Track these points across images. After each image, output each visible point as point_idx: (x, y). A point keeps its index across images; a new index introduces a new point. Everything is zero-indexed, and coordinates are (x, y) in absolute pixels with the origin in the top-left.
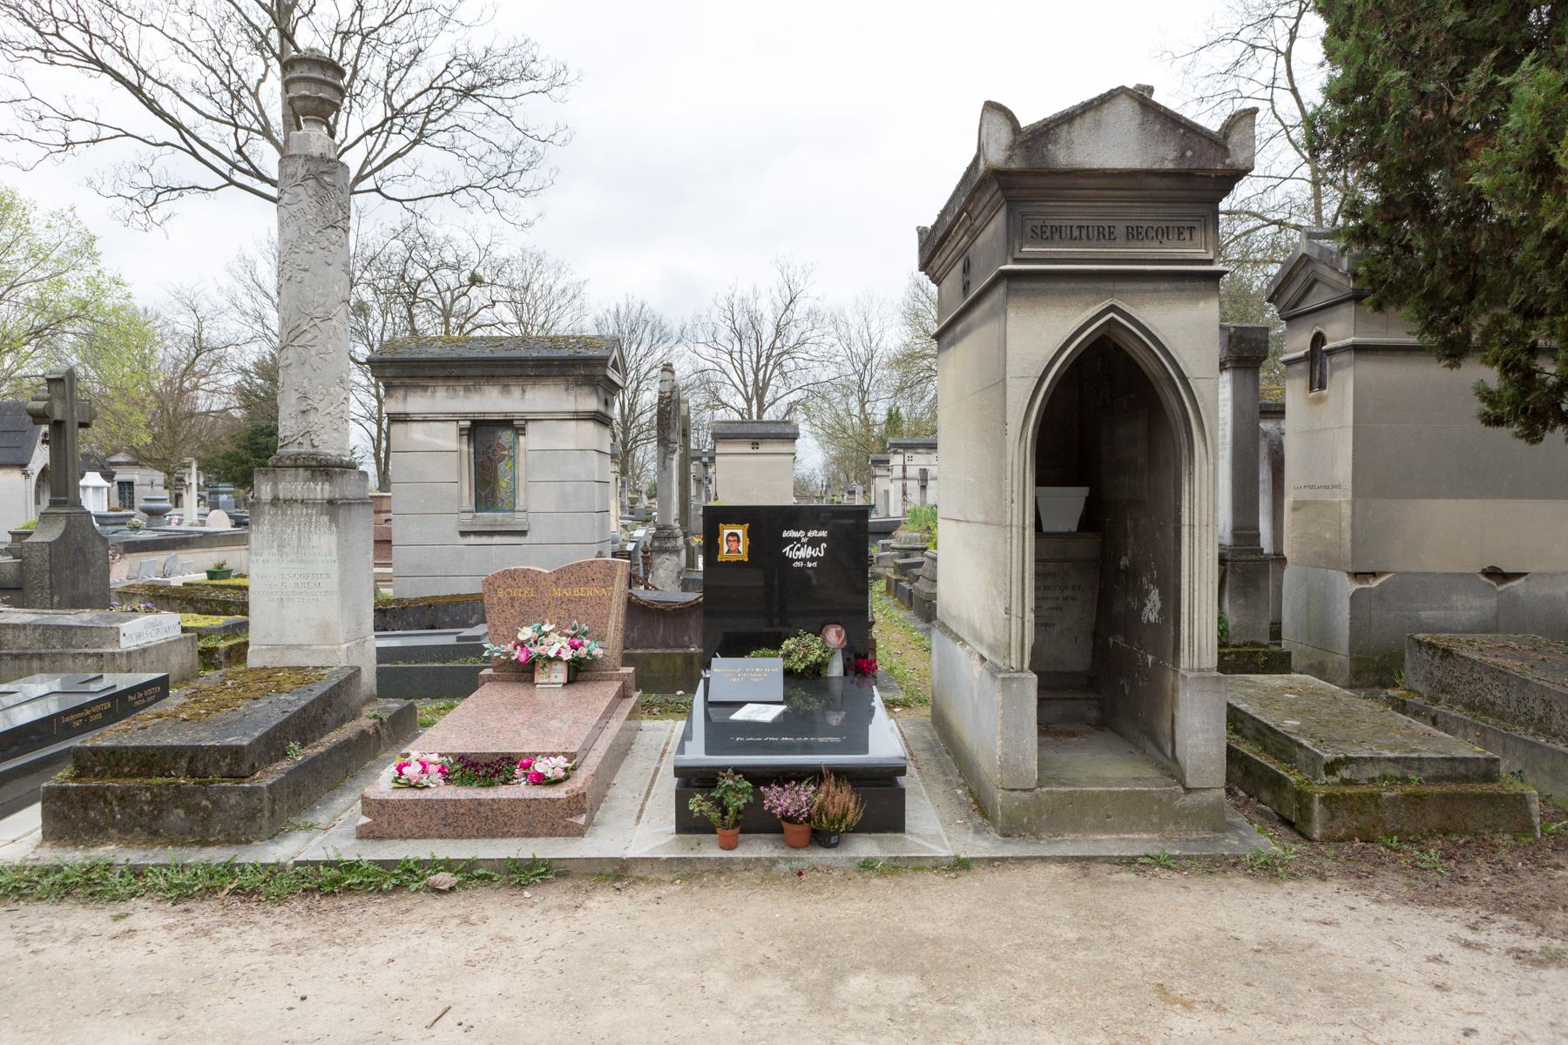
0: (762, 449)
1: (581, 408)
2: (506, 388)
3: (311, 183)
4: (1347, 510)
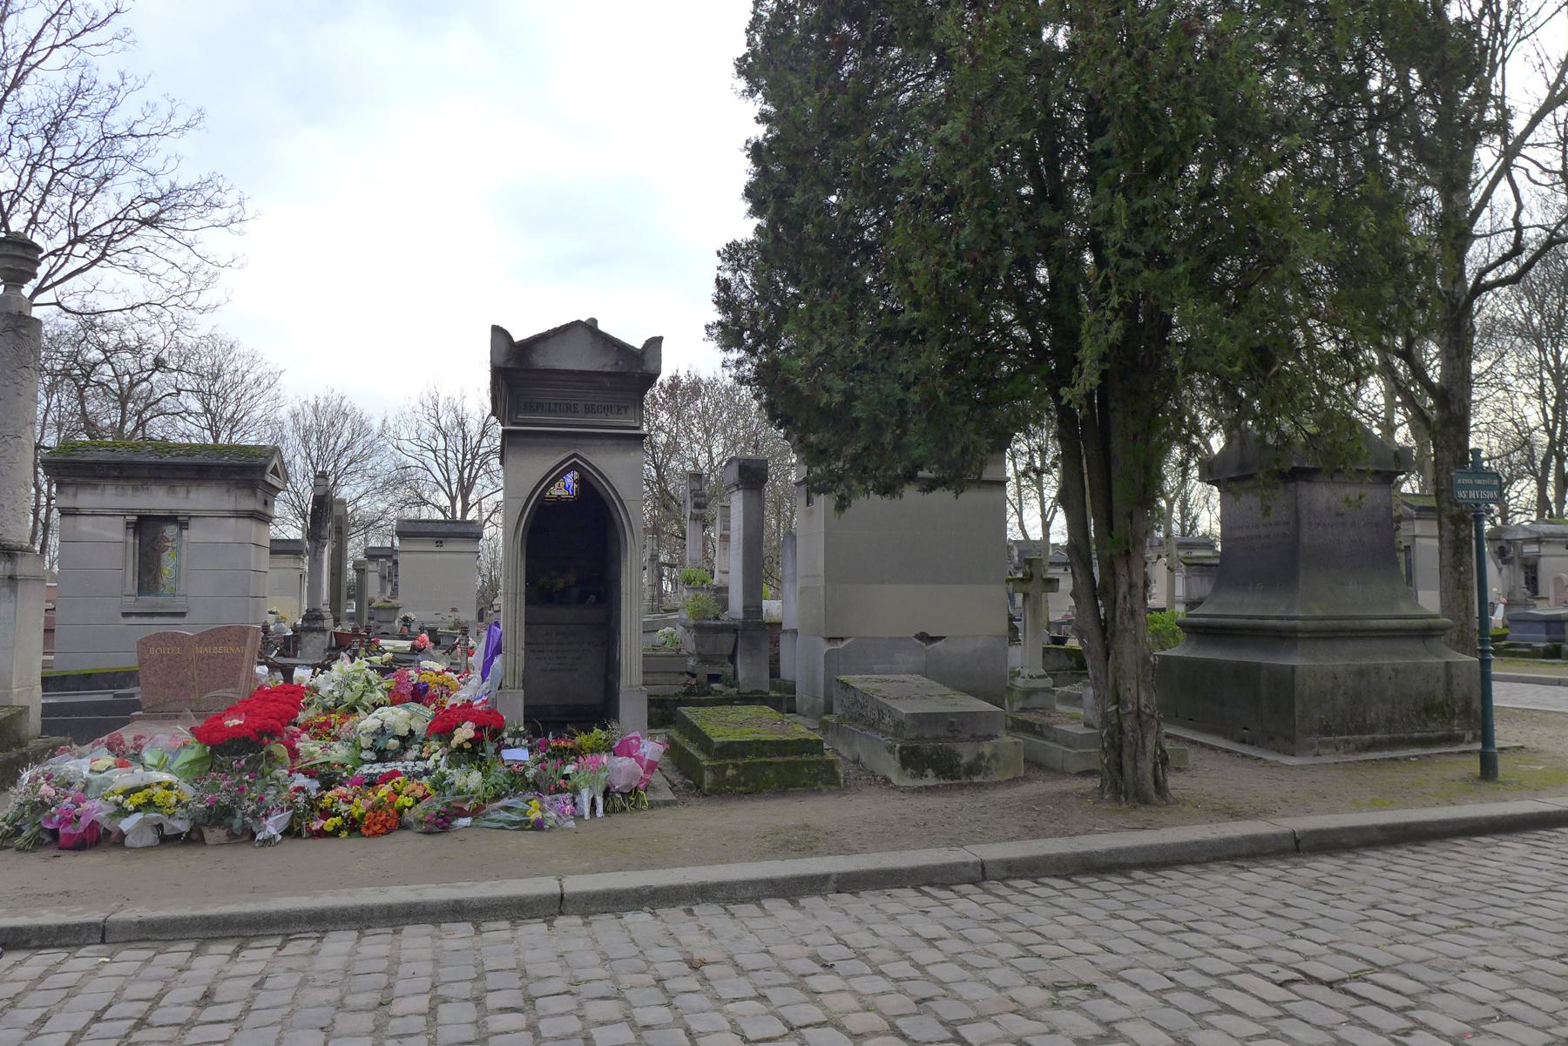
0: (446, 547)
1: (240, 507)
2: (172, 489)
3: (10, 334)
4: (822, 593)
